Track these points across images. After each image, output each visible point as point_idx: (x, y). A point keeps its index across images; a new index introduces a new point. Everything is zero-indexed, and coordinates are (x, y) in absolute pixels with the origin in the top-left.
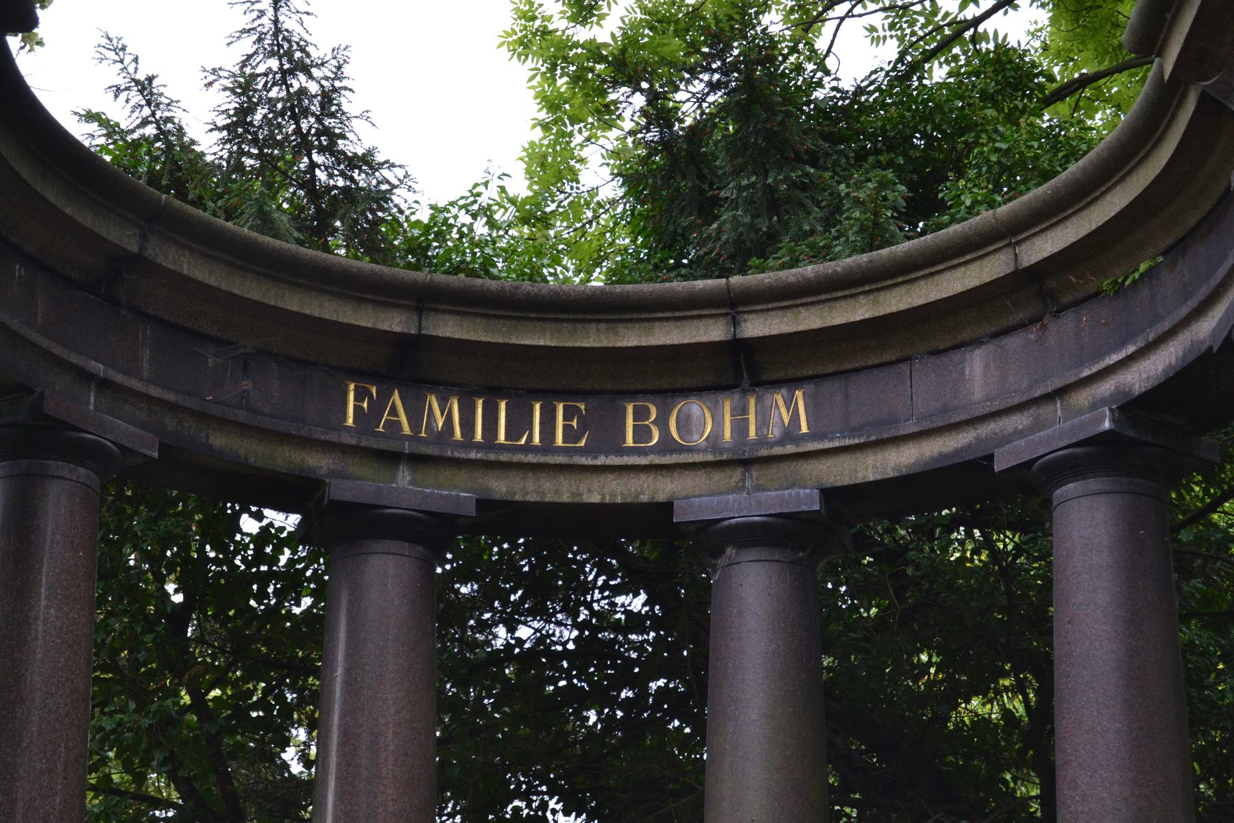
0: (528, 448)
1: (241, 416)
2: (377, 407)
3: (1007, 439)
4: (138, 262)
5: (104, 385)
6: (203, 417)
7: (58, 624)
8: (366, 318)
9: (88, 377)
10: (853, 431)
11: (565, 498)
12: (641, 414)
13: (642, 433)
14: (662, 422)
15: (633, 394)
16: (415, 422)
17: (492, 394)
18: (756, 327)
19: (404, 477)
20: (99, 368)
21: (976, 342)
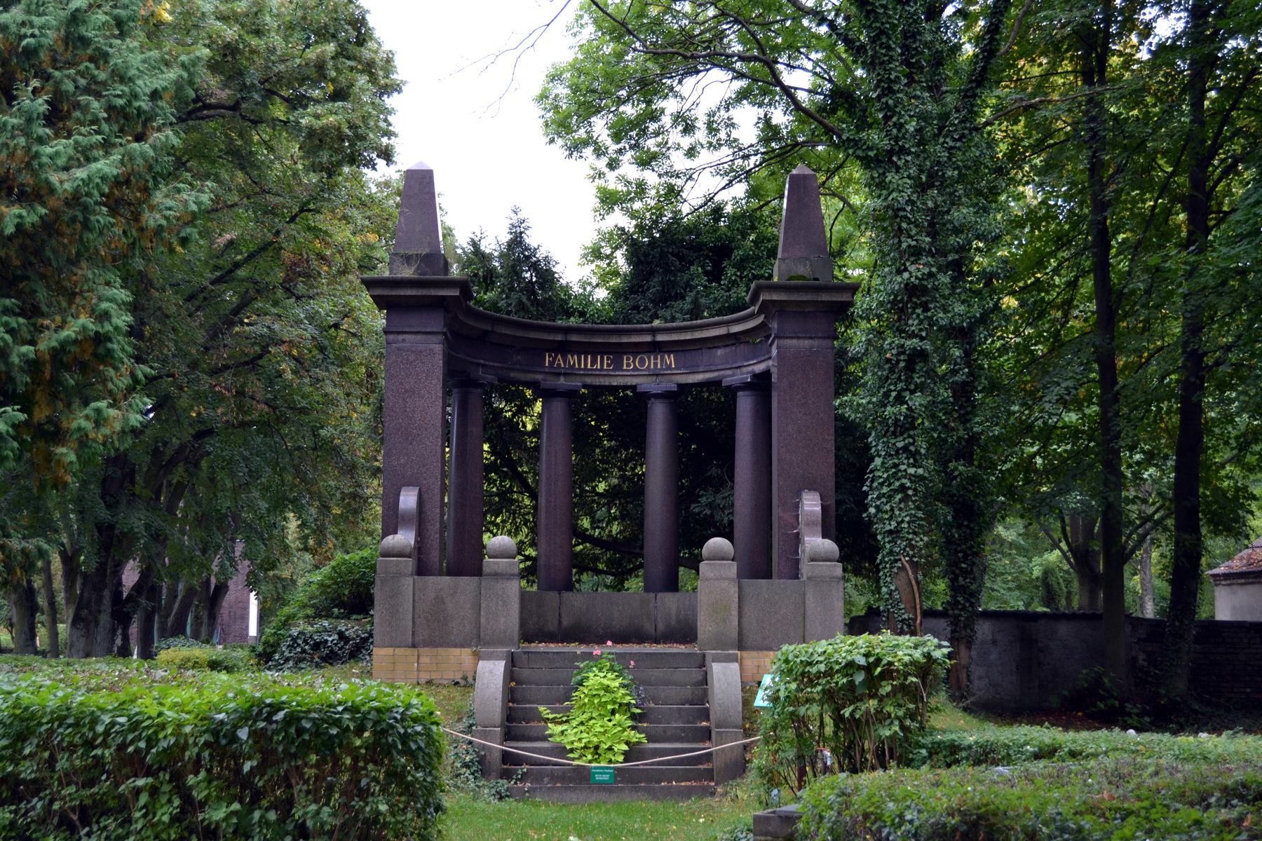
2: (554, 359)
4: (492, 332)
5: (483, 366)
7: (816, 658)
8: (551, 337)
9: (479, 365)
12: (628, 359)
13: (628, 365)
17: (586, 354)
18: (660, 338)
19: (562, 380)
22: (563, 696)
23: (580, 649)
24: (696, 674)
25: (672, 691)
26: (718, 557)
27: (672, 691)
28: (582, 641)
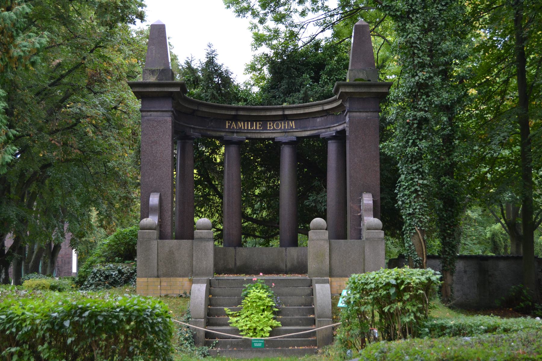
0: (253, 130)
1: (212, 129)
2: (231, 125)
3: (322, 133)
4: (198, 110)
5: (193, 128)
6: (206, 130)
9: (191, 128)
10: (301, 128)
11: (259, 137)
12: (270, 124)
13: (270, 127)
14: (273, 125)
15: (269, 121)
16: (237, 127)
17: (248, 121)
18: (287, 112)
19: (235, 135)
20: (193, 126)
21: (318, 117)
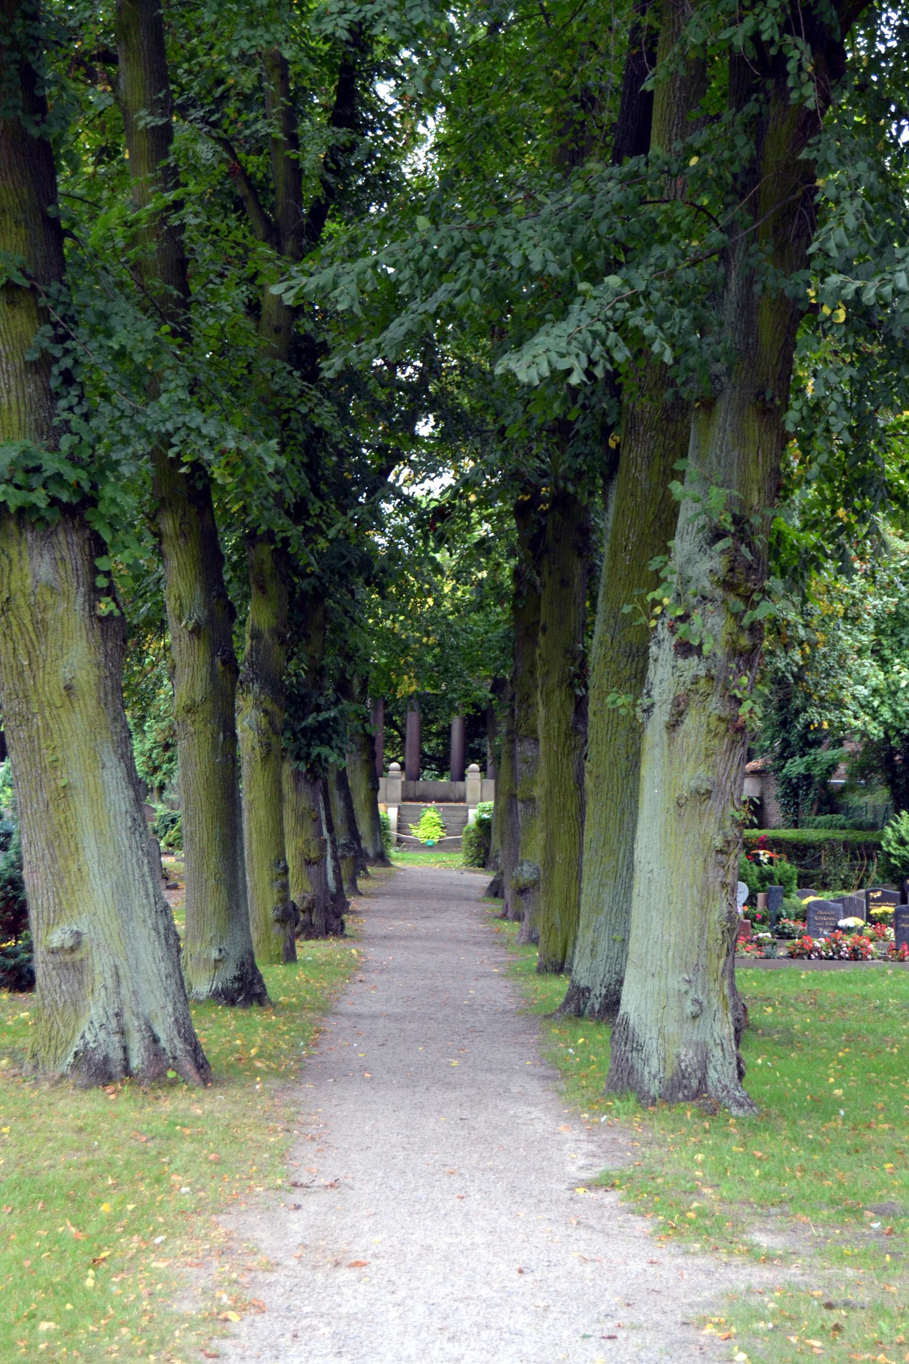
22: (417, 821)
23: (423, 804)
24: (464, 814)
25: (455, 819)
26: (473, 771)
27: (455, 819)
28: (425, 801)
